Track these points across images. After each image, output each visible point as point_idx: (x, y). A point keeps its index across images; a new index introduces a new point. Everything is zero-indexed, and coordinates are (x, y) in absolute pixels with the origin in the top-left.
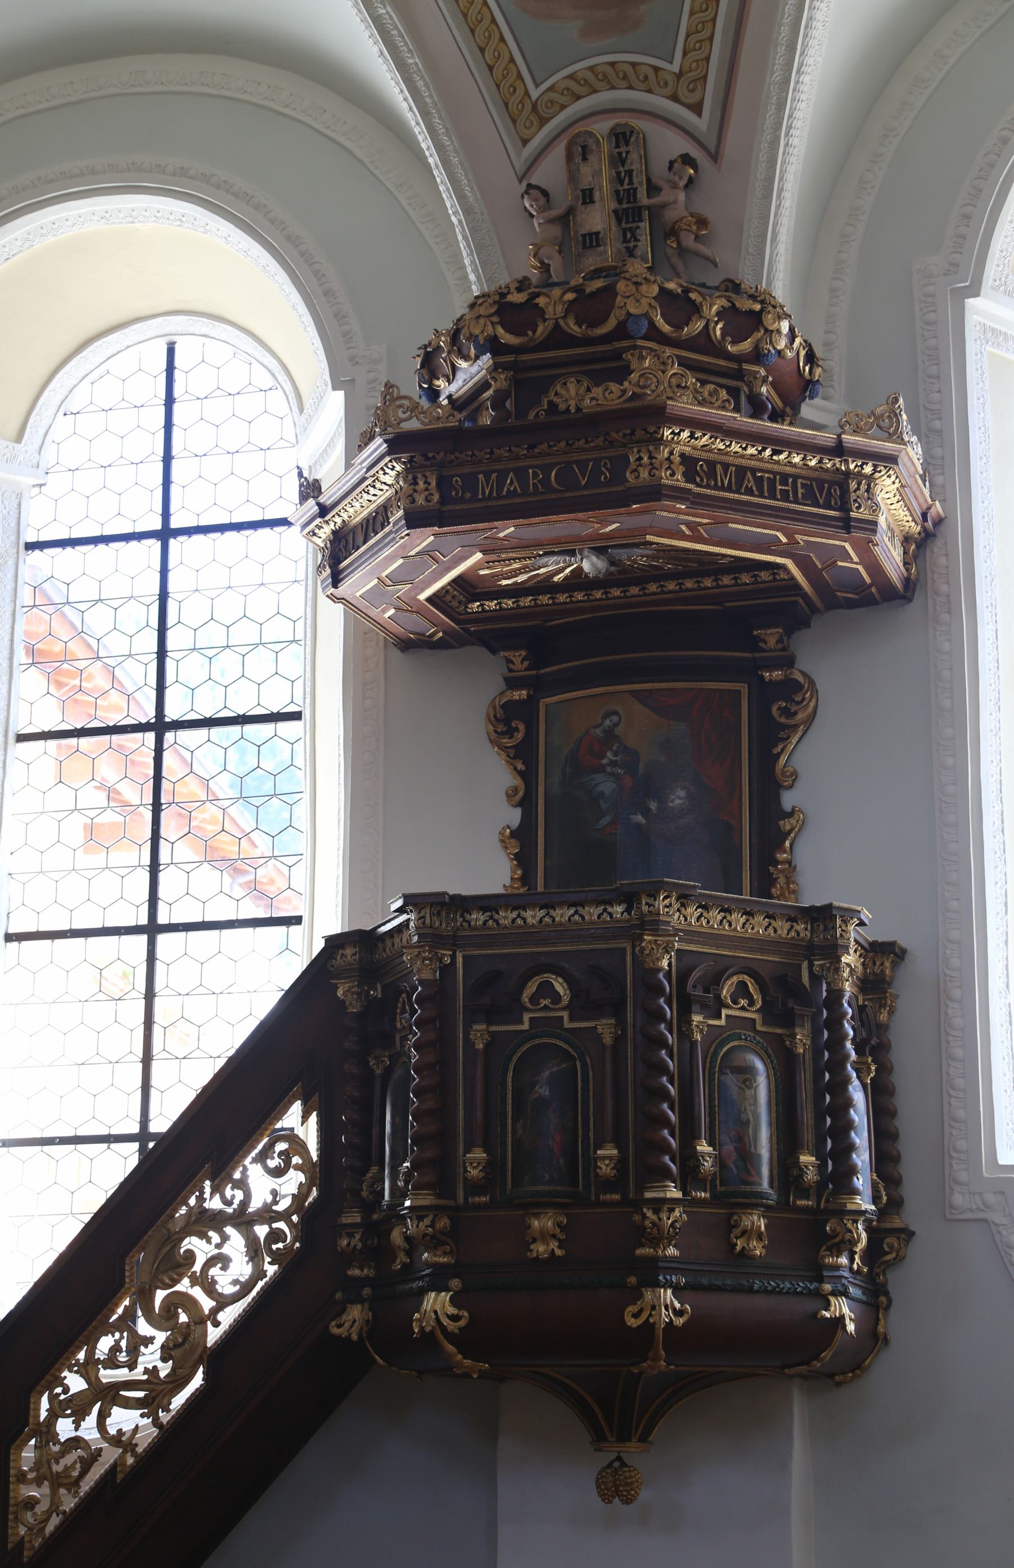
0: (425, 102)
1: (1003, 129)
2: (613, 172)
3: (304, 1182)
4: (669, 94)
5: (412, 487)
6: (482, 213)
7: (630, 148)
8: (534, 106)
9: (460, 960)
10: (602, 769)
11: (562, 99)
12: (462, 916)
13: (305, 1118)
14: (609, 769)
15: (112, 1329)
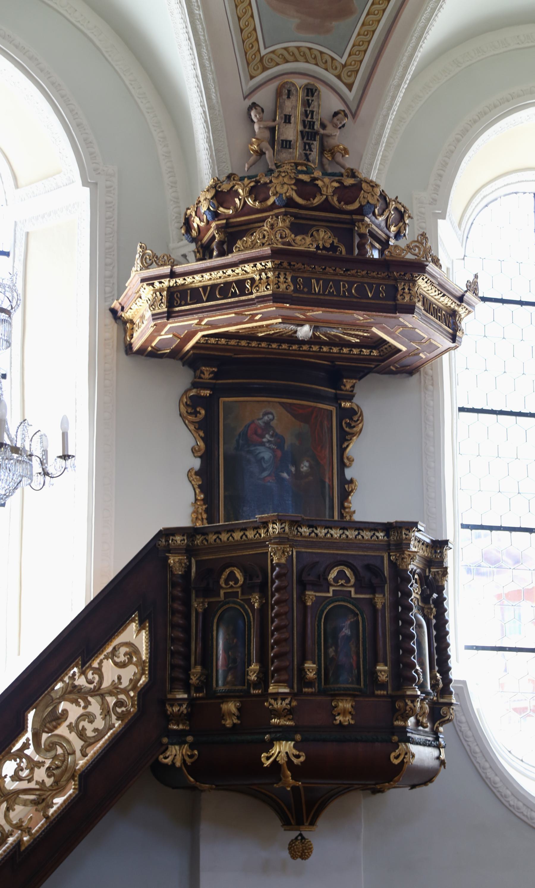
0: (200, 38)
1: (458, 134)
2: (303, 109)
3: (137, 671)
4: (337, 74)
5: (277, 279)
6: (219, 111)
7: (314, 98)
8: (262, 59)
9: (295, 553)
10: (262, 444)
11: (278, 60)
12: (297, 529)
13: (139, 632)
14: (267, 445)
15: (15, 757)
